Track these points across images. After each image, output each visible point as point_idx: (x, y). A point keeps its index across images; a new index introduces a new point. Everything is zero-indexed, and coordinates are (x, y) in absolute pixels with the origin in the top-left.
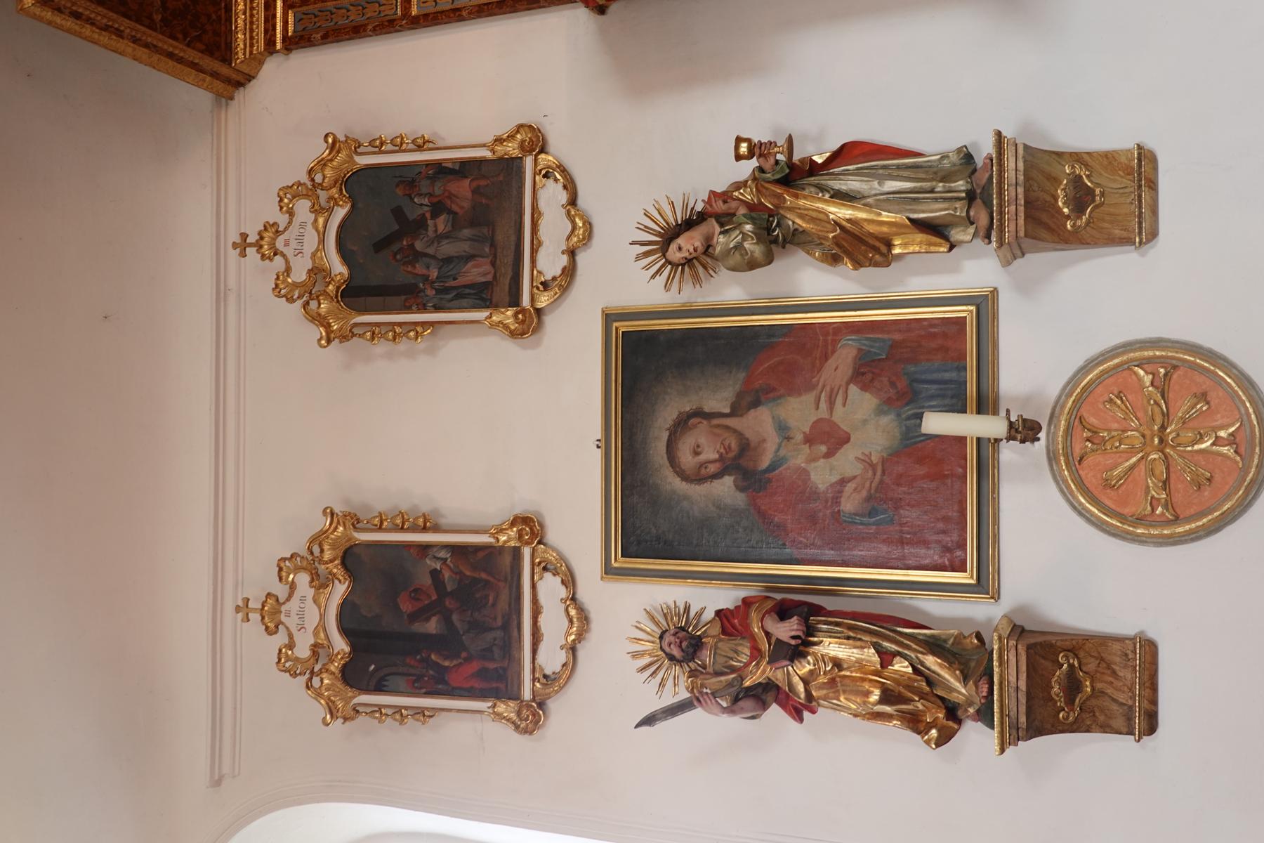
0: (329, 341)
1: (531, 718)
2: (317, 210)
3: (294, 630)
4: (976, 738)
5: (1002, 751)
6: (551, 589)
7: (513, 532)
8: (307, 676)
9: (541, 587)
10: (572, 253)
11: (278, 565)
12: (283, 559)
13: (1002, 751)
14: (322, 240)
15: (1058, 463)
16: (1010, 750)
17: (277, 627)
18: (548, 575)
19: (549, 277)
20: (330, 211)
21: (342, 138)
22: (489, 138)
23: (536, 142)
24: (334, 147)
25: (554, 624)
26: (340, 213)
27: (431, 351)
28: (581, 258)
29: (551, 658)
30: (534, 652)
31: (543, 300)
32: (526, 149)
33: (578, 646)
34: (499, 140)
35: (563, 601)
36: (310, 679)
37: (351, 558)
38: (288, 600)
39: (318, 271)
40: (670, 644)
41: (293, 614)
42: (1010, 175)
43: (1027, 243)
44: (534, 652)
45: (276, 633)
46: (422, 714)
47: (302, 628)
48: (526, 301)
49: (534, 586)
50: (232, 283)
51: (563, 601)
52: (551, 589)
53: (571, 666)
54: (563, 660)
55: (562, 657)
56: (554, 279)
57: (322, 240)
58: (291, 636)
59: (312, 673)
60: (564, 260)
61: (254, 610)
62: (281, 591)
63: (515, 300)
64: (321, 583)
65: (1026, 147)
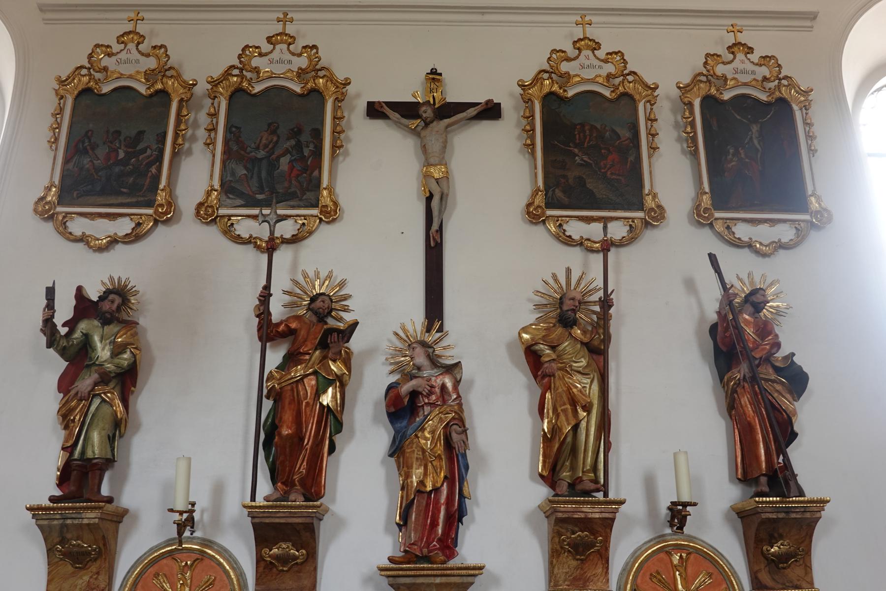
0: (679, 88)
1: (534, 216)
2: (609, 76)
3: (270, 56)
4: (541, 492)
5: (30, 509)
6: (124, 226)
7: (328, 202)
8: (549, 69)
9: (127, 219)
10: (580, 244)
11: (619, 52)
12: (623, 55)
13: (30, 509)
14: (588, 81)
15: (659, 543)
16: (29, 514)
17: (122, 43)
18: (794, 231)
19: (734, 229)
20: (764, 89)
21: (810, 98)
22: (818, 193)
23: (331, 215)
24: (806, 93)
25: (102, 229)
26: (607, 93)
27: (683, 152)
28: (81, 245)
29: (78, 226)
30: (248, 216)
31: (719, 226)
32: (325, 211)
33: (252, 246)
34: (655, 196)
35: (780, 240)
36: (237, 68)
37: (315, 95)
38: (140, 52)
39: (566, 77)
40: (323, 302)
41: (129, 56)
42: (587, 508)
43: (553, 518)
44: (248, 216)
45: (575, 48)
46: (695, 154)
47: (118, 62)
48: (550, 212)
49: (617, 219)
50: (487, 17)
51: (780, 240)
52: (124, 226)
53: (238, 240)
54: (243, 236)
55: (78, 232)
56: (734, 233)
57: (130, 77)
58: (266, 54)
59: (89, 69)
60: (246, 235)
61: (284, 28)
62: (297, 47)
63: (550, 205)
64: (150, 76)
65: (613, 520)
